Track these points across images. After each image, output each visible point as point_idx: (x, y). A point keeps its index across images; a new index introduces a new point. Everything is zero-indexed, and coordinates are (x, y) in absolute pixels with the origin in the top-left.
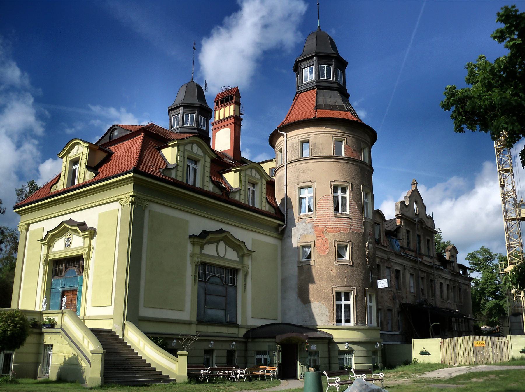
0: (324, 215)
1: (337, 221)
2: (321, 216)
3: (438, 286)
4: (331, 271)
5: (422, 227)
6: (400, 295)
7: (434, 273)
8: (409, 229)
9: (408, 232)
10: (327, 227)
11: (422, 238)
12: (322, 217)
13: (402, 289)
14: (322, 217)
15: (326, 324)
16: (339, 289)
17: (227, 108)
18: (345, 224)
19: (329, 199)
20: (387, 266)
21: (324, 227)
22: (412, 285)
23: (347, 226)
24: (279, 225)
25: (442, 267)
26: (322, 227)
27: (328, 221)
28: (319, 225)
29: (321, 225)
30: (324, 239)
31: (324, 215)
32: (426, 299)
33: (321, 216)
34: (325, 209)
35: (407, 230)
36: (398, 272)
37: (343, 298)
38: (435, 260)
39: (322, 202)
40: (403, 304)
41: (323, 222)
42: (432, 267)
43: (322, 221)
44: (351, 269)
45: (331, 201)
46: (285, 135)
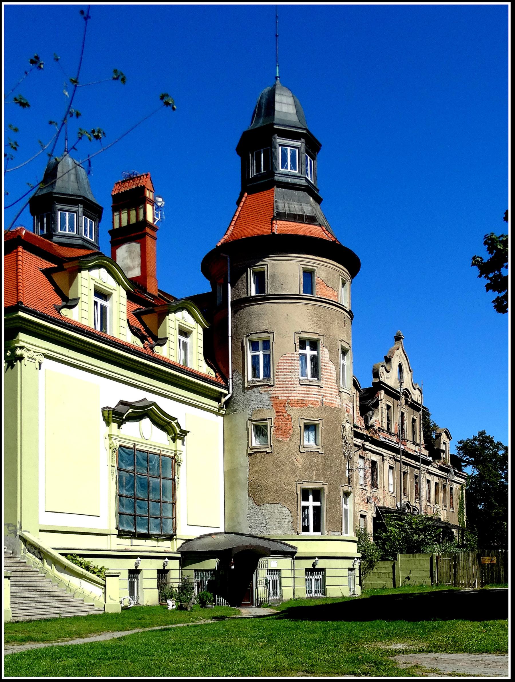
0: (285, 381)
1: (304, 391)
2: (281, 383)
3: (424, 484)
4: (295, 461)
5: (406, 402)
6: (377, 495)
7: (420, 466)
8: (390, 404)
9: (389, 407)
10: (290, 398)
11: (406, 416)
12: (283, 384)
13: (379, 487)
14: (283, 384)
15: (289, 533)
16: (306, 485)
17: (133, 213)
18: (315, 394)
19: (293, 358)
20: (361, 455)
21: (286, 398)
22: (391, 482)
23: (317, 398)
24: (221, 393)
25: (430, 459)
26: (283, 398)
27: (291, 390)
28: (279, 395)
29: (282, 395)
30: (286, 415)
31: (285, 381)
32: (408, 502)
33: (281, 383)
34: (287, 373)
35: (387, 405)
36: (374, 463)
37: (311, 497)
39: (283, 363)
40: (380, 508)
41: (279, 389)
43: (283, 390)
45: (296, 362)
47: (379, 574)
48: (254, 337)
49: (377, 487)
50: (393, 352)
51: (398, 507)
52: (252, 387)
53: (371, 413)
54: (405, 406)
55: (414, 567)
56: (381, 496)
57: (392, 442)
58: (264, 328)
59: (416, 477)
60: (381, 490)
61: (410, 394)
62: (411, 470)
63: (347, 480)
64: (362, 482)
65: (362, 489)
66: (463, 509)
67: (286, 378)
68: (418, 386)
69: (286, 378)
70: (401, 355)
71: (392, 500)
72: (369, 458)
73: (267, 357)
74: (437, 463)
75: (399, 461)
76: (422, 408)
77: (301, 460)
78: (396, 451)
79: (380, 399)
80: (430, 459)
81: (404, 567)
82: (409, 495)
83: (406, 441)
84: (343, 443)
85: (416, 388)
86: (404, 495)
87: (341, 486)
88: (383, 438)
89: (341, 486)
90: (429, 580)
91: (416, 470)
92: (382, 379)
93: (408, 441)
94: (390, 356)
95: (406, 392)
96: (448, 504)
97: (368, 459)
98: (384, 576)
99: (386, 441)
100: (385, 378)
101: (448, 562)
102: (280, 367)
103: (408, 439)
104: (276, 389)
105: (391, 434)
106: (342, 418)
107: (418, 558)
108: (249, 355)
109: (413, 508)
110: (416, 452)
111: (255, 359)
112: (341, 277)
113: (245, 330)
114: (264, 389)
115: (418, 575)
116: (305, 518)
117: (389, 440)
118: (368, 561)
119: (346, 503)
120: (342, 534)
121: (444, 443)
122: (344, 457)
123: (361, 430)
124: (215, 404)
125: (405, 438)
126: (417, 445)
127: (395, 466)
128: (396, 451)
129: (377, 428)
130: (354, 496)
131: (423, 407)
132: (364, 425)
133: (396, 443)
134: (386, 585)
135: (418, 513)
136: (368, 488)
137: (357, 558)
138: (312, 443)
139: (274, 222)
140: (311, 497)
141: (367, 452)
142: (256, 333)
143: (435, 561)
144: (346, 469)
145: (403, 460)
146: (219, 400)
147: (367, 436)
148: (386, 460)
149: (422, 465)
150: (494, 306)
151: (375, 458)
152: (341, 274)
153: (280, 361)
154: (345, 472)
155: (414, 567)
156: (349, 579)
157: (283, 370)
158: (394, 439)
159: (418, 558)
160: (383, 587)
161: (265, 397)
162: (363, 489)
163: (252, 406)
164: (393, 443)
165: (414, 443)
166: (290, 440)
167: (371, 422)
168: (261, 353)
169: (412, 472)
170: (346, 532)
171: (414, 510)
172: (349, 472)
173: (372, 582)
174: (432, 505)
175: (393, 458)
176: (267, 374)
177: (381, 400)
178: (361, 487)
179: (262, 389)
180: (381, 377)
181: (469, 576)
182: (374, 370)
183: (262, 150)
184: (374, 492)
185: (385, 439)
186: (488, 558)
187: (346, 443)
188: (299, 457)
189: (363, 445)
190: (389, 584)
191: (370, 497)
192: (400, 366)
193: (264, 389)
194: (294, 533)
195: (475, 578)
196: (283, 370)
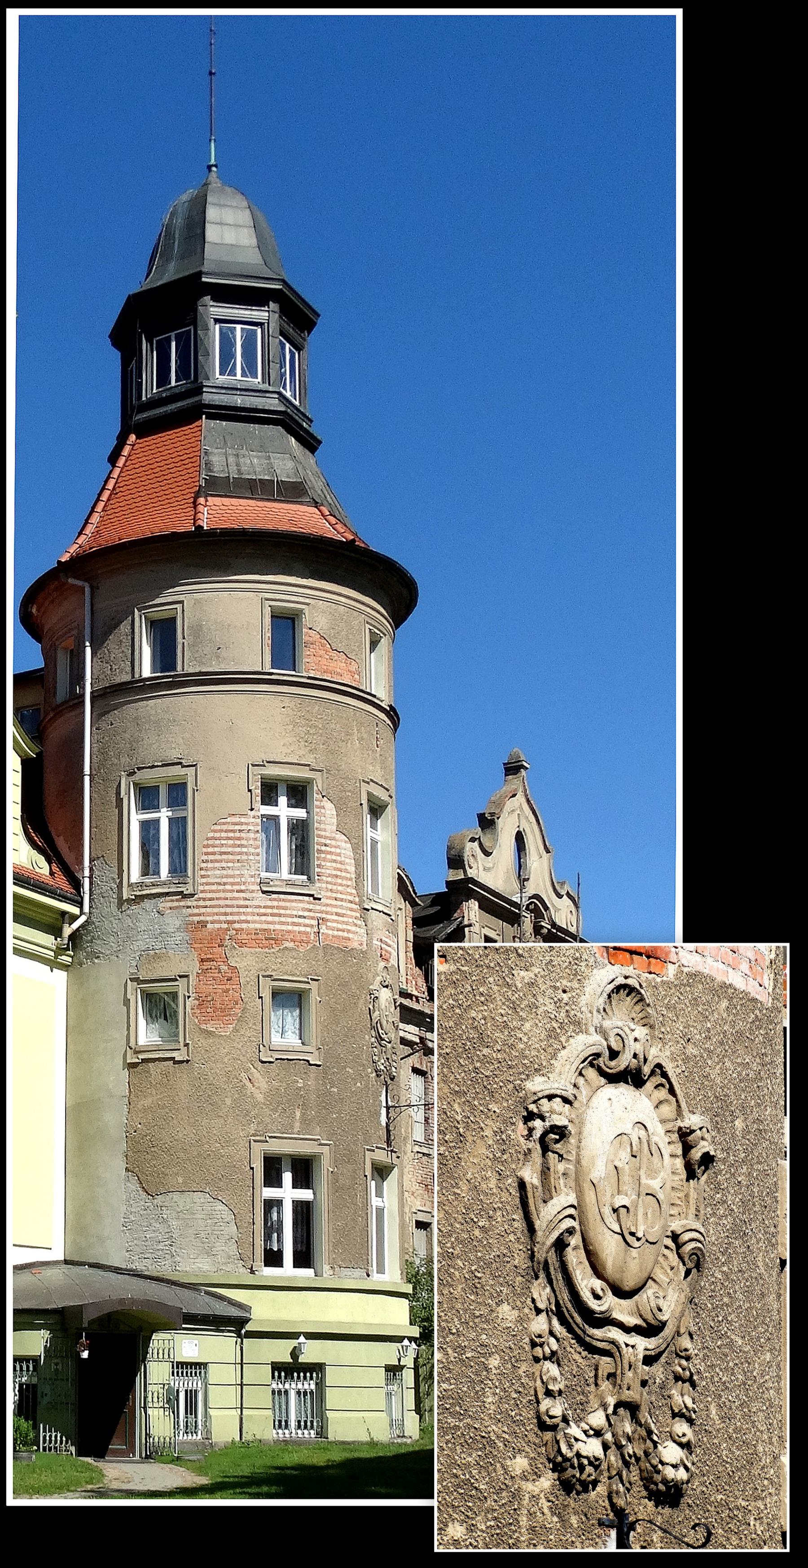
2: (214, 887)
5: (537, 929)
15: (229, 1268)
20: (417, 1066)
28: (208, 918)
30: (224, 968)
33: (214, 887)
37: (287, 1177)
41: (208, 903)
44: (316, 1079)
45: (252, 835)
46: (87, 590)
48: (146, 777)
50: (500, 805)
52: (140, 899)
58: (173, 755)
61: (546, 908)
67: (227, 876)
69: (227, 876)
70: (521, 809)
73: (178, 826)
77: (262, 1082)
79: (466, 922)
84: (373, 1040)
85: (563, 892)
87: (368, 1150)
89: (368, 1150)
92: (471, 873)
94: (492, 814)
95: (536, 904)
100: (481, 868)
102: (210, 850)
104: (201, 903)
108: (135, 818)
111: (149, 830)
112: (368, 626)
113: (125, 760)
114: (170, 904)
116: (272, 1229)
119: (379, 1194)
120: (368, 1275)
124: (48, 940)
130: (401, 1176)
137: (411, 1339)
138: (292, 1040)
139: (202, 500)
140: (287, 1177)
142: (153, 767)
146: (57, 932)
152: (367, 619)
153: (211, 835)
154: (379, 1114)
156: (389, 1395)
157: (218, 857)
161: (173, 922)
162: (424, 1154)
163: (140, 944)
166: (236, 1030)
168: (164, 815)
170: (381, 1270)
172: (388, 1113)
176: (179, 867)
177: (470, 925)
178: (417, 1149)
179: (164, 904)
180: (471, 868)
182: (449, 848)
183: (173, 334)
188: (256, 1074)
192: (520, 838)
193: (170, 904)
194: (242, 1270)
196: (218, 857)
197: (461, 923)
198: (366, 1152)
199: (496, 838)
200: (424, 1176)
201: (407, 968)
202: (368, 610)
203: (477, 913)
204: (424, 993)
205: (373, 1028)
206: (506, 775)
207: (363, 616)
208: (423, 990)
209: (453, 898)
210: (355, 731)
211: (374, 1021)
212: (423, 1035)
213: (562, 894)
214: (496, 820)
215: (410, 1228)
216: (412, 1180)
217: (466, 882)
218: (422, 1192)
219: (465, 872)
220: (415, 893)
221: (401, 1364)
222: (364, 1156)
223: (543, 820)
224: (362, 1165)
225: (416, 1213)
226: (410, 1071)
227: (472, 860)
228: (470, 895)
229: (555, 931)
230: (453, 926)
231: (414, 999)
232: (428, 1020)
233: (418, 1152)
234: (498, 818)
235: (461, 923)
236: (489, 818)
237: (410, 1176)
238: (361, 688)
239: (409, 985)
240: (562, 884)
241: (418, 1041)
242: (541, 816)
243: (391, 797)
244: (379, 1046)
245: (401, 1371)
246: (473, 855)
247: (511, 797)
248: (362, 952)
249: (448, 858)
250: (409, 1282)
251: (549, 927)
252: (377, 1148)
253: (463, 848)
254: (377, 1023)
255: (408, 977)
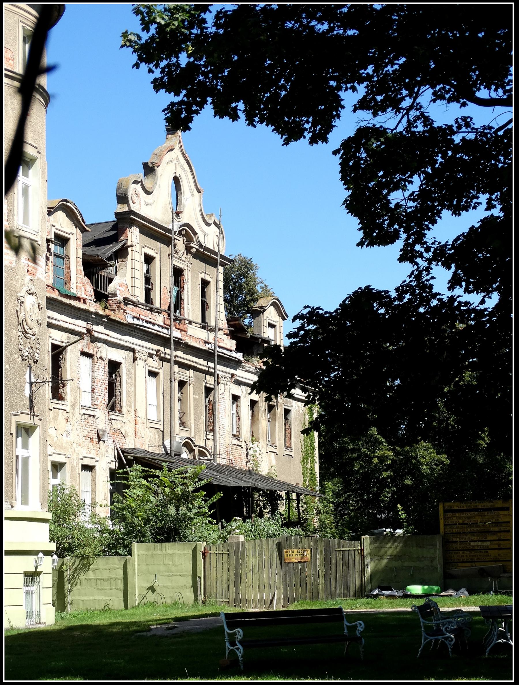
5: (188, 249)
7: (214, 369)
8: (151, 253)
9: (149, 259)
13: (124, 410)
20: (86, 350)
38: (220, 335)
42: (208, 355)
47: (99, 582)
49: (120, 411)
50: (160, 157)
51: (166, 450)
53: (112, 270)
54: (185, 255)
55: (162, 568)
56: (128, 429)
57: (154, 324)
59: (208, 391)
60: (128, 417)
61: (195, 234)
62: (196, 377)
63: (27, 402)
64: (86, 400)
65: (86, 416)
66: (313, 449)
68: (214, 218)
70: (178, 160)
71: (154, 435)
72: (104, 355)
74: (256, 363)
75: (169, 361)
76: (219, 259)
78: (165, 342)
79: (129, 243)
80: (239, 356)
81: (144, 567)
82: (193, 426)
83: (187, 322)
84: (19, 333)
85: (211, 222)
86: (182, 424)
87: (14, 415)
88: (134, 317)
89: (14, 415)
90: (189, 594)
91: (208, 377)
92: (134, 208)
93: (190, 322)
94: (153, 163)
95: (186, 231)
96: (280, 441)
97: (101, 358)
98: (106, 585)
99: (140, 323)
100: (143, 203)
101: (225, 557)
103: (191, 319)
105: (151, 310)
106: (18, 286)
107: (169, 552)
109: (199, 450)
110: (208, 343)
112: (21, 24)
115: (170, 584)
117: (147, 322)
118: (77, 556)
119: (25, 446)
120: (12, 507)
121: (271, 326)
122: (20, 359)
123: (85, 302)
125: (186, 316)
126: (211, 330)
127: (160, 371)
128: (165, 342)
129: (122, 299)
130: (45, 432)
131: (222, 257)
132: (92, 293)
133: (162, 327)
134: (111, 604)
135: (210, 460)
136: (102, 414)
137: (47, 553)
141: (99, 344)
143: (200, 558)
144: (24, 382)
145: (178, 359)
147: (97, 314)
148: (142, 359)
149: (219, 367)
150: (165, 119)
151: (116, 355)
152: (21, 19)
154: (23, 388)
155: (162, 568)
156: (29, 594)
158: (159, 319)
159: (169, 552)
160: (105, 607)
162: (90, 415)
164: (156, 328)
165: (204, 325)
167: (111, 288)
169: (198, 381)
170: (25, 501)
171: (201, 453)
172: (31, 387)
173: (85, 598)
174: (243, 445)
175: (157, 355)
177: (131, 246)
178: (84, 411)
180: (134, 203)
181: (261, 587)
182: (118, 188)
184: (113, 422)
185: (138, 319)
186: (295, 551)
187: (25, 333)
189: (89, 331)
190: (117, 603)
191: (104, 431)
192: (176, 180)
195: (272, 590)
197: (125, 244)
198: (12, 416)
199: (155, 182)
200: (89, 431)
201: (77, 278)
202: (22, 12)
203: (138, 237)
204: (91, 296)
205: (19, 324)
206: (167, 134)
207: (18, 16)
208: (90, 294)
209: (120, 226)
210: (9, 103)
211: (21, 320)
212: (90, 327)
213: (210, 223)
214: (156, 168)
215: (77, 470)
216: (80, 434)
217: (128, 214)
218: (87, 444)
219: (129, 206)
220: (84, 223)
221: (38, 570)
222: (11, 419)
223: (195, 169)
224: (9, 426)
225: (82, 459)
226: (80, 354)
227: (135, 197)
228: (132, 223)
229: (202, 250)
230: (119, 246)
231: (82, 301)
232: (93, 316)
233: (84, 414)
234: (158, 167)
235: (125, 244)
236: (151, 166)
237: (78, 432)
238: (14, 70)
239: (78, 290)
240: (211, 215)
241: (86, 332)
242: (194, 166)
243: (39, 153)
244: (24, 338)
245: (39, 576)
246: (136, 194)
247: (169, 151)
248: (12, 269)
249: (117, 195)
250: (50, 511)
251: (198, 247)
252: (21, 413)
253: (128, 189)
254: (23, 321)
255: (78, 284)
